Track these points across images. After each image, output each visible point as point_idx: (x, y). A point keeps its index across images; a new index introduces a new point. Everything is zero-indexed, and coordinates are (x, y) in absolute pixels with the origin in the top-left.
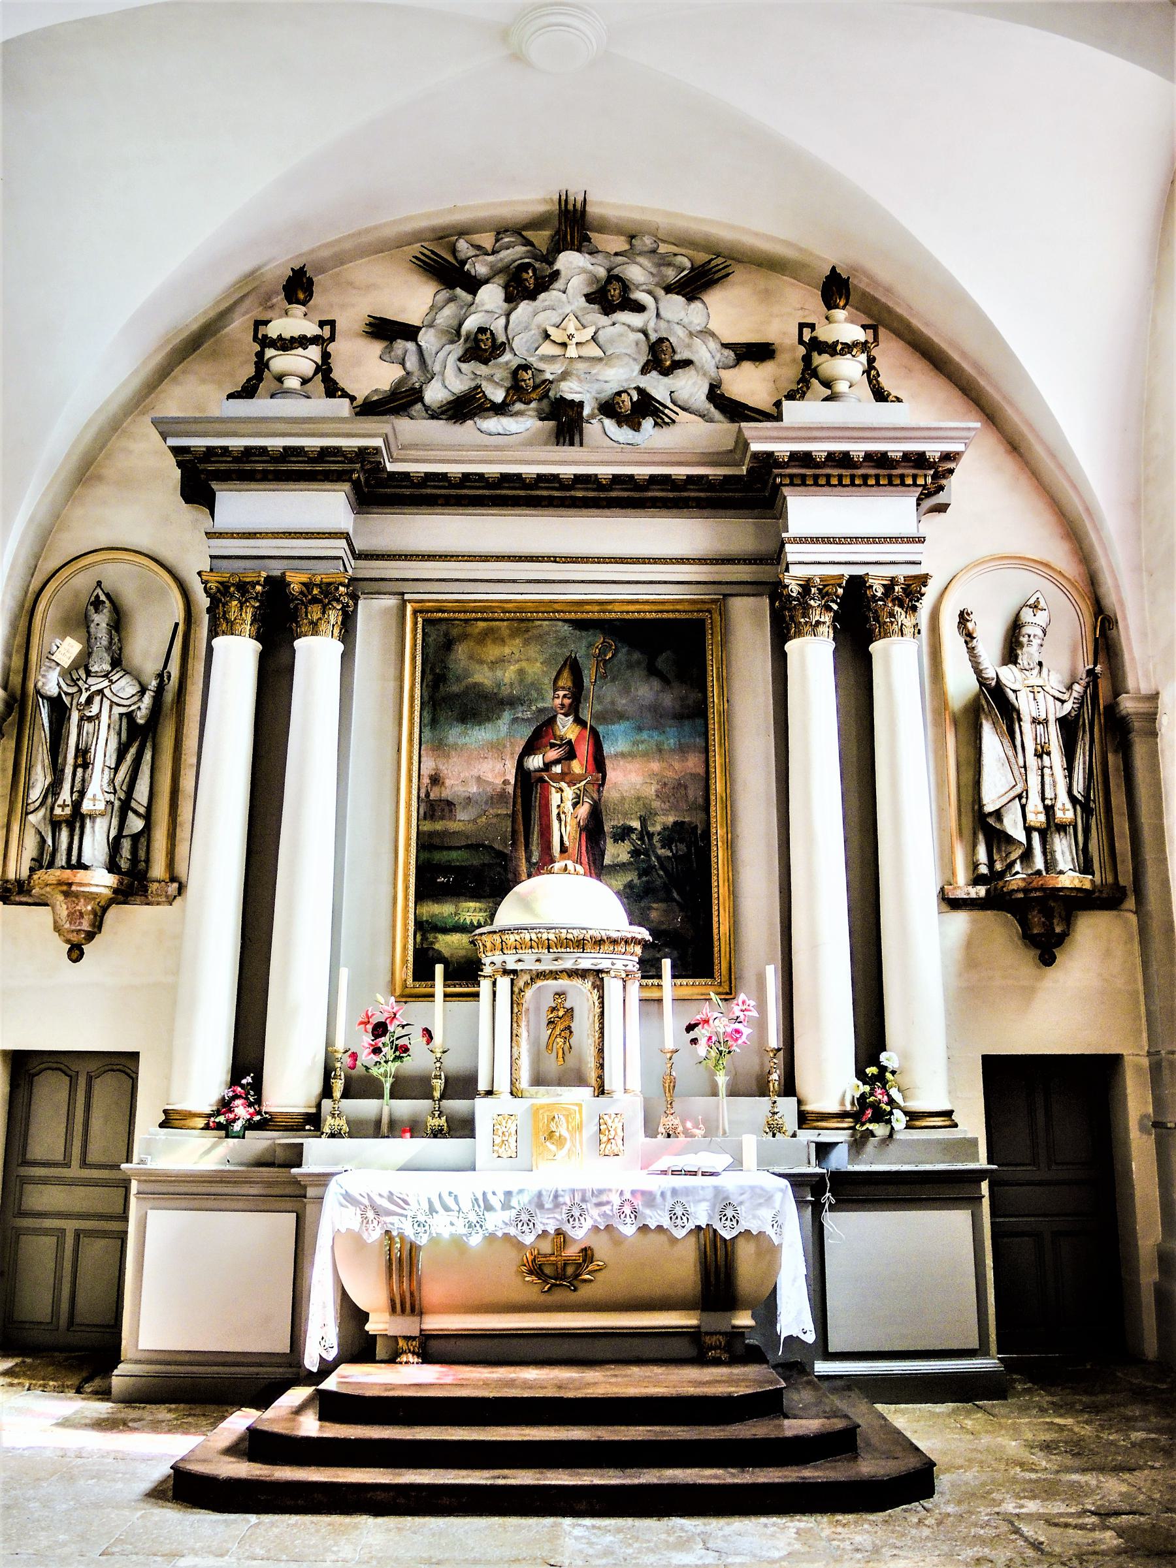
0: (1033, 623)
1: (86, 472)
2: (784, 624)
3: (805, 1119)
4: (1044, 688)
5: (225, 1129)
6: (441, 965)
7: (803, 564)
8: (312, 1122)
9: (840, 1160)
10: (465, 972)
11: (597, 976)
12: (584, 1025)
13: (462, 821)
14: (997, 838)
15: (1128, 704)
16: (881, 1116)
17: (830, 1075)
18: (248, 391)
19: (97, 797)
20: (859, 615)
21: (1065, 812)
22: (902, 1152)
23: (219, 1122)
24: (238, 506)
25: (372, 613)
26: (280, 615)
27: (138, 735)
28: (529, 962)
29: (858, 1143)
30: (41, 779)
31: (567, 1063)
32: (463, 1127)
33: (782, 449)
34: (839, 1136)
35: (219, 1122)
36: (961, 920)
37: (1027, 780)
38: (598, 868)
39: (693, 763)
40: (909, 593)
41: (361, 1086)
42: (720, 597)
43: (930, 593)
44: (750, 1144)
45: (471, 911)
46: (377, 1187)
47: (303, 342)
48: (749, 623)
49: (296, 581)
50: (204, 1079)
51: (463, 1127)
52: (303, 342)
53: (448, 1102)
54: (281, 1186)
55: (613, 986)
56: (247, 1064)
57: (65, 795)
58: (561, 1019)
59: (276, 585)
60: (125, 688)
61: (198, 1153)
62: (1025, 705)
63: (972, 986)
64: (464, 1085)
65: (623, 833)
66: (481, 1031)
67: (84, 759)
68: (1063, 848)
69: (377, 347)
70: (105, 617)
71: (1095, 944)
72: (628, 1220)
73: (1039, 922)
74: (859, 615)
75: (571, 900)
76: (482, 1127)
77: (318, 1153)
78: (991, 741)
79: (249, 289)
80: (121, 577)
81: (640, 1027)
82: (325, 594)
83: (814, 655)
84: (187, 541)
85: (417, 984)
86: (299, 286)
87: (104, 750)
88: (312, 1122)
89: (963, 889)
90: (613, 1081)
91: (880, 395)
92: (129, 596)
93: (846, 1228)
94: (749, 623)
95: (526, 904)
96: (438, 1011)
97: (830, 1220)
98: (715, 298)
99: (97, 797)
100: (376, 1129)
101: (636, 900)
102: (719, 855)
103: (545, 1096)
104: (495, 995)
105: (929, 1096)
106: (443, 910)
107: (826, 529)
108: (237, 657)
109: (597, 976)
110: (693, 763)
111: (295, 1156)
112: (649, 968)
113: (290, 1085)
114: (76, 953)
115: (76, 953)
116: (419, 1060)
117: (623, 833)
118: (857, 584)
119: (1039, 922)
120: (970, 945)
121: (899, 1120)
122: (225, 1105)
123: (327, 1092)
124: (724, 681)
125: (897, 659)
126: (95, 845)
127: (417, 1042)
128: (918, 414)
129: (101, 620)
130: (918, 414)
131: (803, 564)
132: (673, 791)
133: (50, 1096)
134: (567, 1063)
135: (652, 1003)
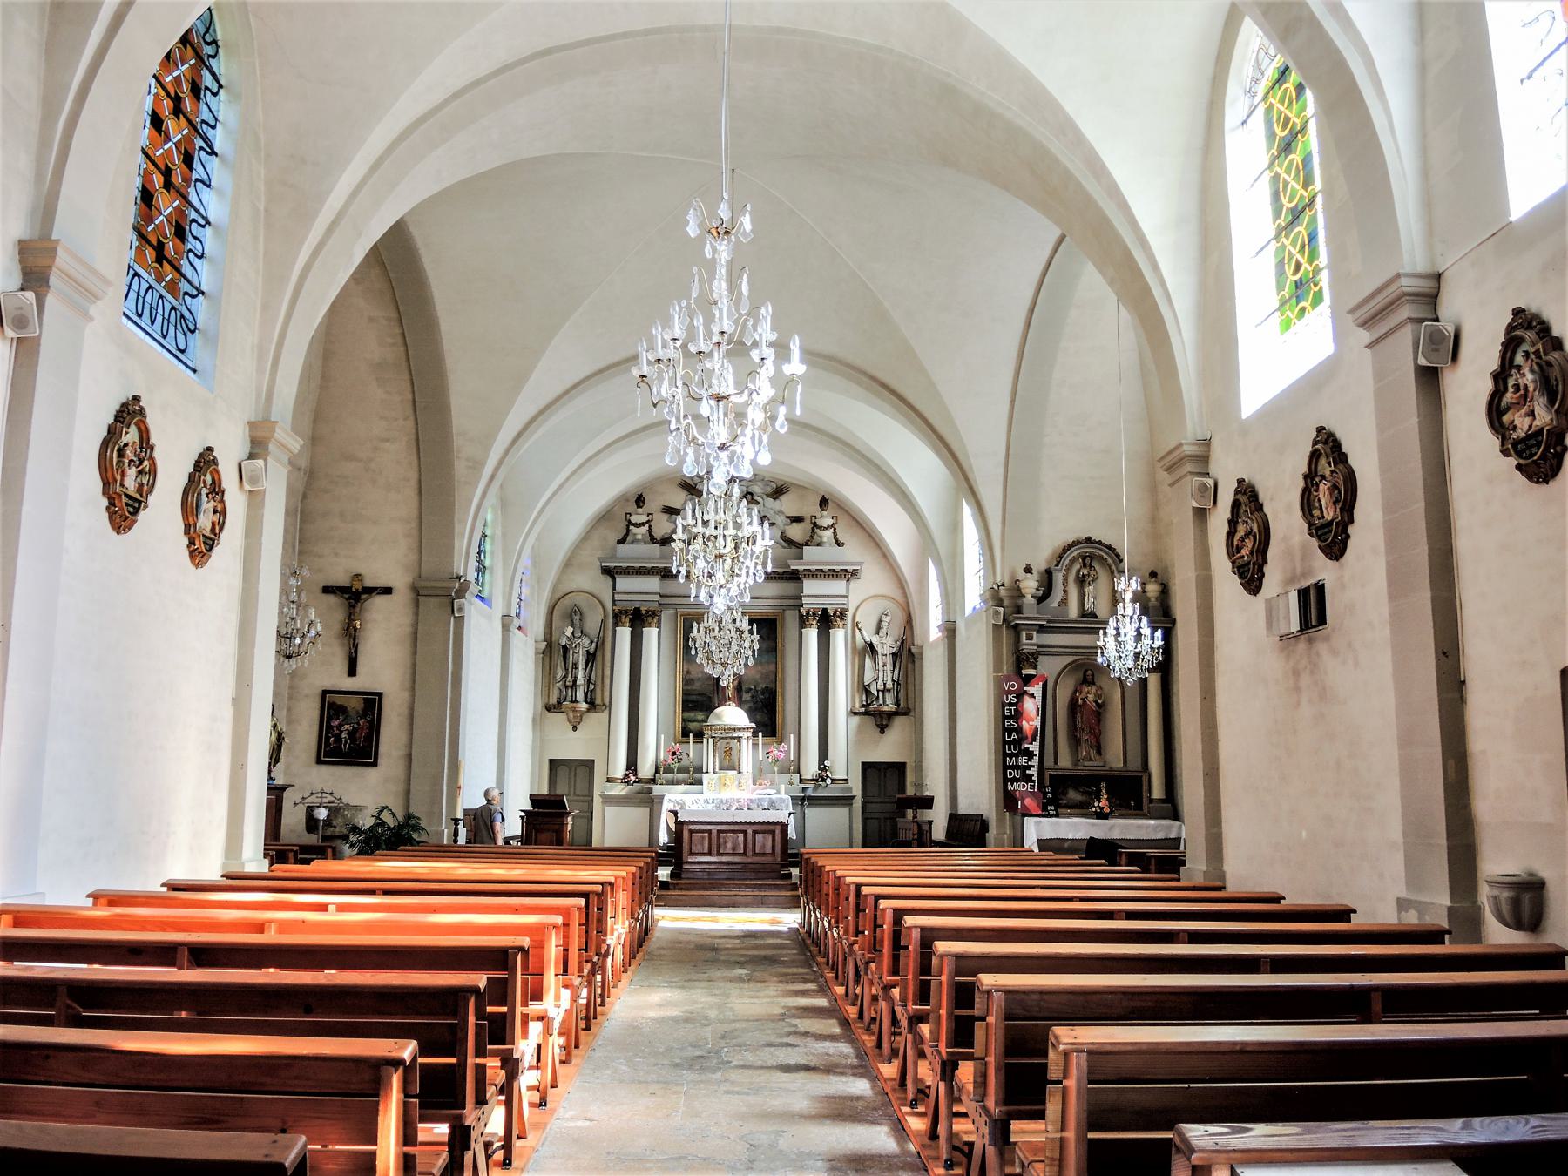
0: (886, 620)
1: (568, 564)
2: (803, 622)
3: (801, 781)
4: (886, 646)
5: (628, 783)
6: (691, 732)
7: (808, 603)
8: (653, 781)
9: (809, 793)
10: (699, 735)
11: (739, 739)
12: (735, 752)
13: (696, 686)
14: (868, 692)
15: (914, 650)
16: (823, 780)
17: (811, 768)
18: (621, 542)
19: (580, 680)
20: (826, 621)
21: (890, 685)
22: (829, 790)
23: (625, 780)
24: (623, 583)
25: (666, 616)
26: (639, 619)
27: (591, 658)
28: (718, 734)
29: (817, 787)
30: (560, 673)
31: (730, 763)
32: (700, 782)
33: (801, 568)
34: (810, 786)
35: (625, 780)
36: (857, 718)
37: (881, 675)
38: (740, 704)
39: (772, 667)
40: (842, 614)
41: (668, 770)
42: (784, 608)
43: (850, 614)
44: (782, 787)
45: (700, 715)
46: (677, 799)
47: (642, 524)
48: (791, 620)
49: (643, 609)
50: (620, 769)
51: (700, 782)
52: (642, 524)
53: (693, 774)
54: (645, 796)
55: (744, 742)
56: (632, 764)
57: (570, 678)
58: (729, 751)
59: (637, 610)
60: (586, 641)
61: (619, 790)
62: (879, 649)
63: (859, 740)
64: (699, 770)
65: (749, 690)
66: (709, 755)
67: (575, 666)
68: (889, 698)
69: (666, 516)
70: (575, 615)
71: (899, 726)
72: (709, 365)
73: (882, 721)
74: (826, 621)
75: (732, 715)
76: (705, 782)
77: (657, 790)
78: (868, 662)
79: (622, 499)
80: (581, 600)
81: (749, 753)
82: (653, 614)
83: (812, 635)
84: (603, 586)
85: (1052, 1108)
86: (640, 501)
87: (581, 665)
88: (653, 781)
89: (858, 708)
90: (743, 768)
91: (838, 544)
92: (583, 606)
93: (811, 813)
94: (791, 620)
95: (719, 717)
96: (691, 747)
97: (807, 811)
98: (783, 498)
99: (580, 680)
100: (673, 783)
101: (751, 713)
102: (779, 698)
103: (723, 774)
104: (708, 745)
105: (840, 774)
106: (691, 715)
107: (816, 593)
108: (624, 633)
109: (739, 739)
110: (772, 667)
111: (651, 790)
112: (755, 734)
113: (646, 769)
114: (575, 728)
115: (575, 728)
116: (685, 762)
117: (749, 690)
118: (825, 610)
119: (882, 721)
120: (859, 726)
121: (829, 781)
122: (626, 776)
123: (657, 771)
124: (783, 639)
125: (839, 636)
126: (580, 695)
127: (684, 757)
128: (852, 553)
129: (577, 618)
130: (852, 553)
131: (808, 603)
132: (765, 676)
133: (562, 773)
134: (730, 763)
135: (755, 745)
